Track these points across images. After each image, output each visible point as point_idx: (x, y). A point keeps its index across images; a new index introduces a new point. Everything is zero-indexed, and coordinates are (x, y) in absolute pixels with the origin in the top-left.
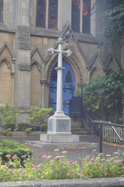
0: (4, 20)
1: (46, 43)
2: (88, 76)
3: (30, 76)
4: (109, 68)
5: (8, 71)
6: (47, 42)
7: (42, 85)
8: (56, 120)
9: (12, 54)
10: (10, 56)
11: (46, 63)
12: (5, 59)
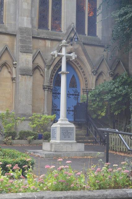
0: (4, 22)
1: (49, 46)
2: (94, 81)
3: (32, 81)
4: (116, 72)
5: (9, 75)
6: (50, 44)
7: (44, 91)
8: (59, 128)
9: (13, 57)
10: (11, 60)
11: (49, 67)
12: (6, 63)
